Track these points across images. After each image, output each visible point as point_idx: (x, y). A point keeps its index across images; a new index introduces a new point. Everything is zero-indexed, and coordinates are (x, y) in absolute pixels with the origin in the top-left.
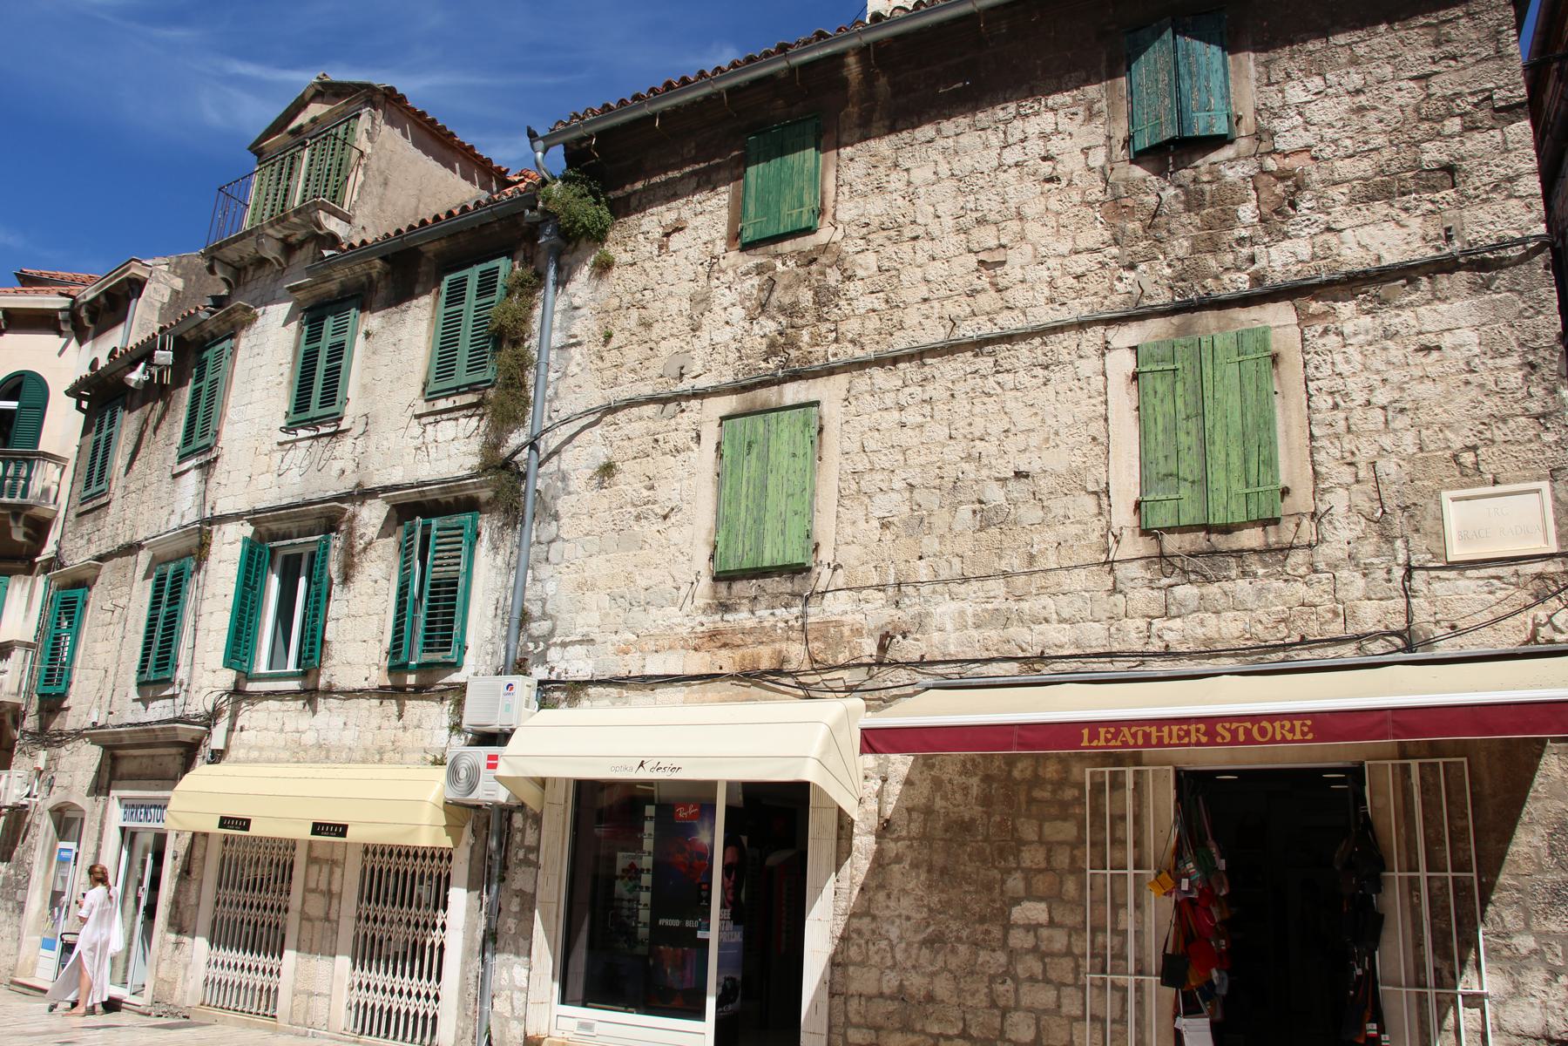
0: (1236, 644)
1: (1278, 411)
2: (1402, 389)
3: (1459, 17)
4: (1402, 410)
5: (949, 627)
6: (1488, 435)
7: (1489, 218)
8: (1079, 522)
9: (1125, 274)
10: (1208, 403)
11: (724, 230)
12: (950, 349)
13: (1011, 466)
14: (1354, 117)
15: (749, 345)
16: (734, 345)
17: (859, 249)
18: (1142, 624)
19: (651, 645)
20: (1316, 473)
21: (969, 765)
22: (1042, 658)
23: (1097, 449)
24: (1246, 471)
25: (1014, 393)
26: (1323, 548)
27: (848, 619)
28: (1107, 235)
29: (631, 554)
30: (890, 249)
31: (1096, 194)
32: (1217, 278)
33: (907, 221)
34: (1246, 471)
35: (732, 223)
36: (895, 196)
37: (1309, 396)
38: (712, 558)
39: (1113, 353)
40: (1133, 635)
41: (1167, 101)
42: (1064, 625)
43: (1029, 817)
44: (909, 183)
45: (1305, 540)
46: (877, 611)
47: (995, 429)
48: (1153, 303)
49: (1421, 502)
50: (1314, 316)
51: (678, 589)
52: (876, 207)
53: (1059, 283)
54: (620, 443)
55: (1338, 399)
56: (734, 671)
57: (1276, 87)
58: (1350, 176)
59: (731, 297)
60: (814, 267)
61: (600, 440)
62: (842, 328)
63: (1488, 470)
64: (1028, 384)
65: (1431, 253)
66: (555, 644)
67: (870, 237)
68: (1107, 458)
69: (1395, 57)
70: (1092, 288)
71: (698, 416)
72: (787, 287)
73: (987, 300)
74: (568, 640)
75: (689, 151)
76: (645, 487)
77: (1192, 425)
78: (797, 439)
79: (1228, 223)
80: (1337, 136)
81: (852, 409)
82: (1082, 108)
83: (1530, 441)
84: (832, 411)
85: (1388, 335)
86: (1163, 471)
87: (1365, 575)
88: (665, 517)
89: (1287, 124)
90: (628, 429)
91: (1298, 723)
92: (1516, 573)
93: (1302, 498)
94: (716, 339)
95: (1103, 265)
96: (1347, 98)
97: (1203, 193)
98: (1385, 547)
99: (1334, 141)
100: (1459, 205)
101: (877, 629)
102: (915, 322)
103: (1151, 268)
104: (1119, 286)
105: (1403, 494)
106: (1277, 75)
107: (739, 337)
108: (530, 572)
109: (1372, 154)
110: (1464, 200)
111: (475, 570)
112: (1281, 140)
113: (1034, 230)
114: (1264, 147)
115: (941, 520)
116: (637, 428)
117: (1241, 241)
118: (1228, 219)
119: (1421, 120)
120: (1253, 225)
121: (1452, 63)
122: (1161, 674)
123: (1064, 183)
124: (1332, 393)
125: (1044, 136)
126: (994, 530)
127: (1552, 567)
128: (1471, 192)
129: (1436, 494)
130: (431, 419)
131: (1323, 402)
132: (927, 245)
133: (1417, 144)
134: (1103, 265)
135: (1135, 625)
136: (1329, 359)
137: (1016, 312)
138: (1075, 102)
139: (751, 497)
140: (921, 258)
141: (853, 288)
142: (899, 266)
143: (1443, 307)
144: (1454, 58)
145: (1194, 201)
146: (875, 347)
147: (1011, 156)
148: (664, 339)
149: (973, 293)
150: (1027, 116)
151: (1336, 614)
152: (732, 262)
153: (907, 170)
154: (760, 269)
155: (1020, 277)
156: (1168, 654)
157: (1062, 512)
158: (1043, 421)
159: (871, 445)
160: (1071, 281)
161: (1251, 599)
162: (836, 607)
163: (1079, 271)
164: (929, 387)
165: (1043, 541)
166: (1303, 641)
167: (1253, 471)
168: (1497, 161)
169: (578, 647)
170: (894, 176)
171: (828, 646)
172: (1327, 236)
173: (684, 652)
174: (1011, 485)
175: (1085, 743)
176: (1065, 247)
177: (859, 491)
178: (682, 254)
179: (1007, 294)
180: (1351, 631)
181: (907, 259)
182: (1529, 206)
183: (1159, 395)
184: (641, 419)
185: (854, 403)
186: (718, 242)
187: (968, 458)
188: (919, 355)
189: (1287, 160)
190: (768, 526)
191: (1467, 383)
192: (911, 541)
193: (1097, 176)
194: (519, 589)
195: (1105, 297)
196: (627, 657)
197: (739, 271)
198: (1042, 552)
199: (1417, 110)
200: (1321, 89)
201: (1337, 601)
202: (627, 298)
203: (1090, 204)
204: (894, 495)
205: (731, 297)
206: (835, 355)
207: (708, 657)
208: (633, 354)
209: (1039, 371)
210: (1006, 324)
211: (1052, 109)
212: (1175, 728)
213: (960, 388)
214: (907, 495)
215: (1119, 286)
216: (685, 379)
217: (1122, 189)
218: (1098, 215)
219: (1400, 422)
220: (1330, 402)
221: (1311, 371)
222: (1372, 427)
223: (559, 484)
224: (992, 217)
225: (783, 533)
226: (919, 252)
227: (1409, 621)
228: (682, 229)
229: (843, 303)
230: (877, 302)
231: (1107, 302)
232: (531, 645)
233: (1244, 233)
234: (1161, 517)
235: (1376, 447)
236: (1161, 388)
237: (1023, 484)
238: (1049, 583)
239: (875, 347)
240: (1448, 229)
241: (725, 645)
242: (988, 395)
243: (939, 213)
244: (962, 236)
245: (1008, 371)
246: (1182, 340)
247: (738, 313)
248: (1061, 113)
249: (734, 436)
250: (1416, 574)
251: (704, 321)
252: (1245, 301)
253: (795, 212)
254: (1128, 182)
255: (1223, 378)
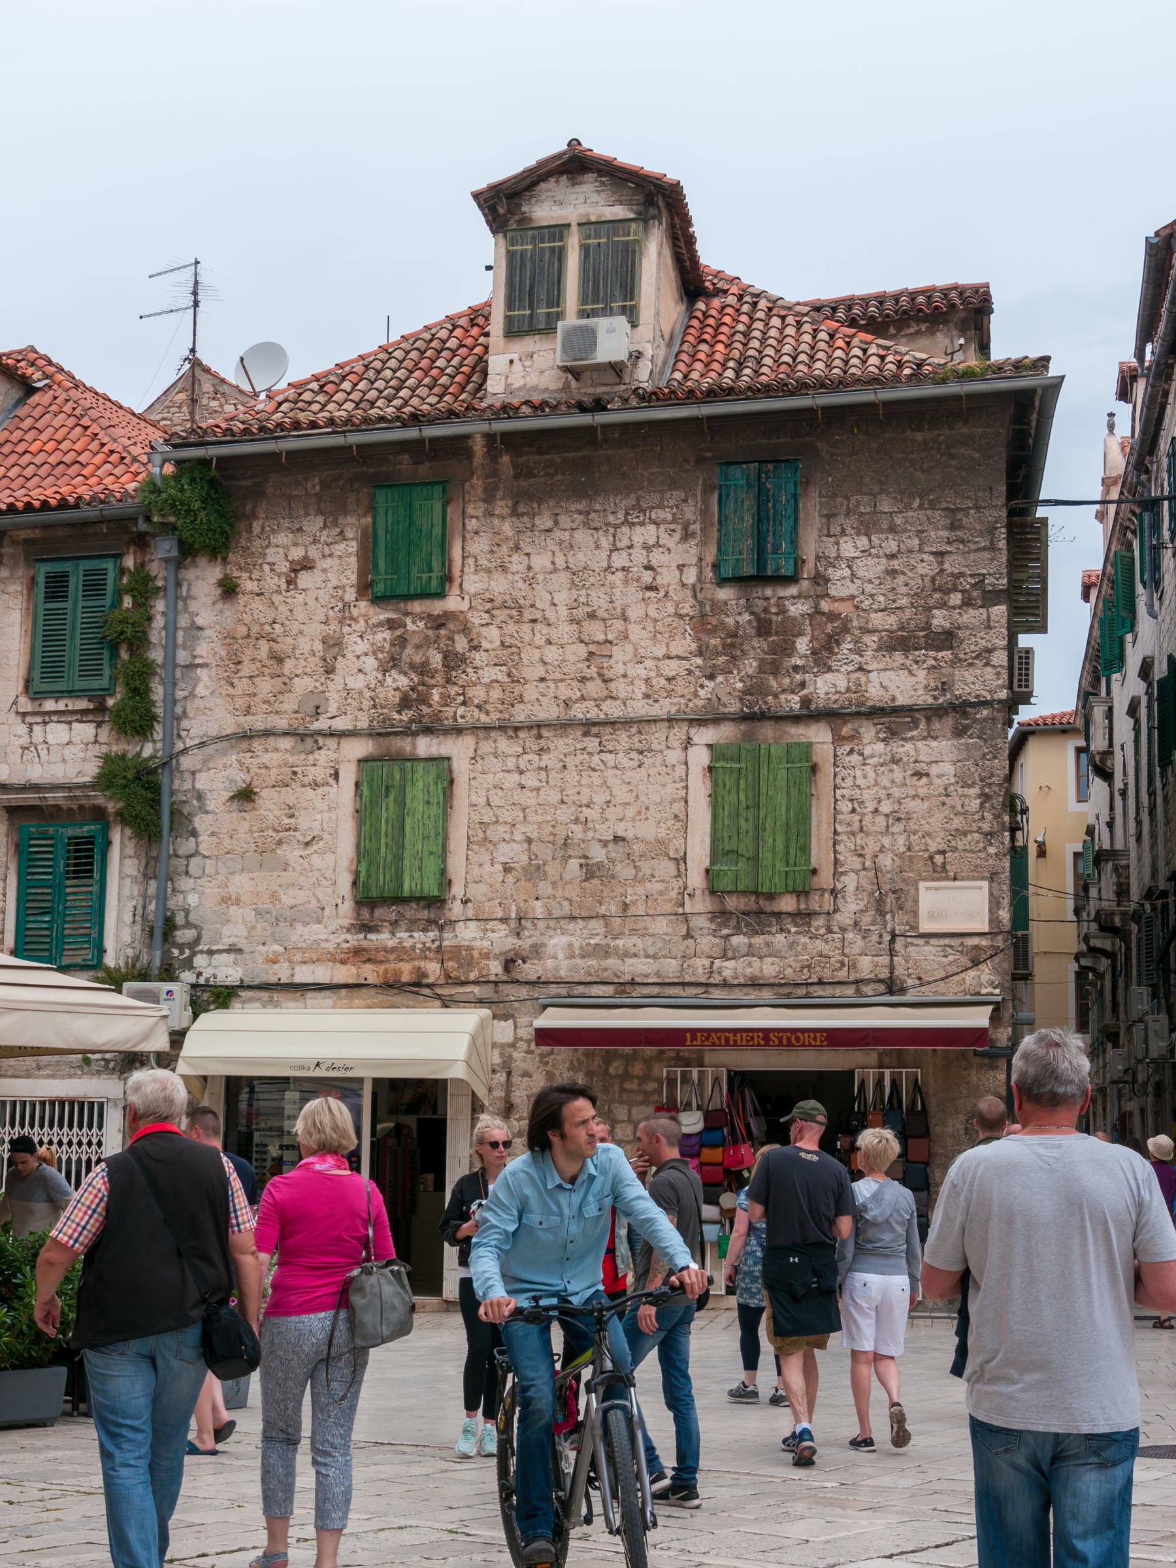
0: (772, 981)
1: (814, 809)
2: (900, 804)
3: (970, 508)
4: (899, 819)
5: (561, 956)
6: (953, 843)
7: (971, 679)
8: (662, 881)
9: (707, 683)
10: (763, 799)
11: (354, 578)
12: (563, 726)
13: (611, 831)
14: (888, 578)
15: (382, 695)
16: (367, 694)
17: (484, 622)
18: (707, 962)
19: (298, 957)
20: (836, 861)
21: (575, 1063)
22: (633, 983)
23: (678, 825)
24: (787, 853)
25: (615, 771)
26: (838, 916)
27: (477, 944)
28: (694, 646)
29: (275, 874)
30: (512, 628)
31: (687, 608)
32: (776, 696)
33: (528, 603)
34: (787, 853)
35: (362, 572)
36: (517, 577)
37: (836, 801)
38: (355, 883)
39: (694, 748)
40: (700, 971)
41: (750, 541)
42: (649, 960)
43: (621, 1102)
44: (529, 568)
45: (826, 909)
46: (500, 939)
47: (600, 799)
48: (726, 711)
49: (906, 888)
50: (844, 738)
51: (323, 909)
52: (499, 585)
53: (654, 682)
54: (258, 771)
55: (856, 805)
56: (377, 982)
57: (832, 540)
58: (881, 628)
59: (362, 647)
60: (443, 632)
61: (236, 765)
62: (470, 693)
63: (951, 870)
64: (627, 765)
65: (930, 701)
66: (201, 952)
67: (495, 612)
68: (686, 831)
69: (922, 532)
70: (680, 690)
71: (336, 755)
72: (418, 647)
73: (594, 688)
74: (214, 948)
75: (314, 486)
76: (286, 815)
77: (751, 814)
78: (431, 788)
79: (788, 652)
80: (874, 591)
81: (478, 767)
82: (680, 527)
83: (980, 851)
84: (461, 767)
85: (895, 761)
86: (727, 848)
87: (864, 938)
88: (307, 844)
89: (839, 574)
90: (266, 758)
91: (818, 1035)
92: (962, 944)
93: (825, 878)
94: (351, 685)
95: (690, 672)
96: (884, 561)
97: (770, 622)
98: (879, 918)
99: (872, 596)
100: (953, 664)
101: (501, 954)
102: (534, 698)
103: (727, 681)
104: (702, 693)
105: (894, 881)
106: (835, 530)
107: (373, 686)
108: (169, 883)
109: (898, 613)
110: (956, 662)
111: (109, 878)
112: (833, 587)
113: (634, 631)
114: (819, 590)
115: (552, 869)
116: (272, 758)
117: (796, 668)
118: (787, 649)
119: (934, 590)
120: (806, 656)
121: (961, 546)
122: (718, 1003)
123: (662, 594)
124: (851, 800)
125: (647, 548)
126: (596, 882)
127: (984, 942)
128: (962, 656)
129: (916, 883)
130: (39, 719)
131: (845, 806)
132: (545, 630)
133: (930, 609)
134: (690, 672)
135: (701, 963)
136: (852, 773)
137: (619, 702)
138: (674, 520)
139: (390, 836)
140: (539, 640)
141: (479, 658)
142: (519, 645)
143: (934, 744)
144: (962, 541)
145: (763, 628)
146: (499, 715)
147: (619, 560)
148: (297, 676)
149: (583, 680)
150: (633, 524)
151: (843, 964)
152: (363, 611)
153: (528, 554)
154: (391, 625)
155: (622, 672)
156: (725, 985)
157: (649, 872)
158: (637, 797)
159: (495, 801)
160: (663, 682)
161: (786, 949)
162: (467, 934)
163: (671, 674)
164: (545, 757)
165: (635, 893)
166: (820, 983)
167: (792, 854)
168: (982, 634)
169: (225, 955)
170: (515, 558)
171: (461, 966)
172: (859, 674)
173: (331, 964)
174: (611, 846)
175: (688, 1043)
176: (660, 651)
177: (485, 839)
178: (312, 594)
179: (612, 685)
180: (852, 978)
181: (527, 639)
182: (998, 674)
183: (728, 787)
184: (277, 750)
185: (480, 762)
186: (348, 588)
187: (577, 821)
188: (538, 727)
189: (836, 605)
190: (407, 862)
191: (944, 804)
192: (529, 885)
193: (689, 593)
194: (162, 898)
195: (690, 700)
196: (276, 966)
197: (370, 622)
198: (634, 902)
199: (933, 580)
200: (867, 548)
201: (844, 954)
202: (255, 629)
203: (681, 617)
204: (515, 846)
205: (362, 647)
206: (463, 717)
207: (354, 970)
208: (265, 686)
209: (634, 755)
210: (610, 711)
211: (655, 523)
212: (744, 1035)
213: (571, 761)
214: (526, 846)
215: (702, 693)
216: (322, 718)
217: (708, 608)
218: (688, 627)
219: (898, 828)
220: (850, 807)
221: (838, 781)
222: (878, 829)
223: (195, 802)
224: (601, 613)
225: (420, 869)
226: (538, 635)
227: (891, 973)
228: (311, 568)
229: (469, 670)
230: (499, 674)
231: (691, 705)
232: (176, 952)
233: (800, 662)
234: (725, 883)
235: (879, 844)
236: (729, 782)
237: (620, 847)
238: (638, 926)
239: (499, 715)
240: (943, 683)
241: (369, 960)
242: (594, 770)
243: (556, 601)
244: (575, 627)
245: (610, 752)
246: (747, 745)
247: (370, 663)
248: (662, 527)
249: (372, 779)
250: (898, 939)
251: (337, 666)
252: (796, 719)
253: (425, 576)
254: (714, 603)
255: (775, 779)
